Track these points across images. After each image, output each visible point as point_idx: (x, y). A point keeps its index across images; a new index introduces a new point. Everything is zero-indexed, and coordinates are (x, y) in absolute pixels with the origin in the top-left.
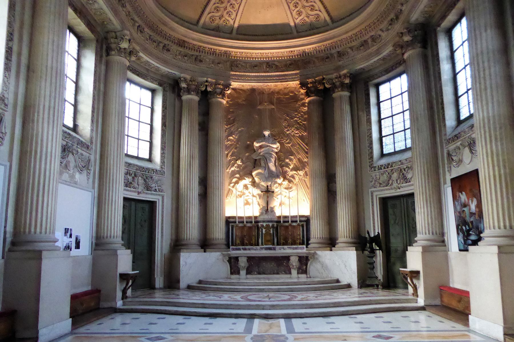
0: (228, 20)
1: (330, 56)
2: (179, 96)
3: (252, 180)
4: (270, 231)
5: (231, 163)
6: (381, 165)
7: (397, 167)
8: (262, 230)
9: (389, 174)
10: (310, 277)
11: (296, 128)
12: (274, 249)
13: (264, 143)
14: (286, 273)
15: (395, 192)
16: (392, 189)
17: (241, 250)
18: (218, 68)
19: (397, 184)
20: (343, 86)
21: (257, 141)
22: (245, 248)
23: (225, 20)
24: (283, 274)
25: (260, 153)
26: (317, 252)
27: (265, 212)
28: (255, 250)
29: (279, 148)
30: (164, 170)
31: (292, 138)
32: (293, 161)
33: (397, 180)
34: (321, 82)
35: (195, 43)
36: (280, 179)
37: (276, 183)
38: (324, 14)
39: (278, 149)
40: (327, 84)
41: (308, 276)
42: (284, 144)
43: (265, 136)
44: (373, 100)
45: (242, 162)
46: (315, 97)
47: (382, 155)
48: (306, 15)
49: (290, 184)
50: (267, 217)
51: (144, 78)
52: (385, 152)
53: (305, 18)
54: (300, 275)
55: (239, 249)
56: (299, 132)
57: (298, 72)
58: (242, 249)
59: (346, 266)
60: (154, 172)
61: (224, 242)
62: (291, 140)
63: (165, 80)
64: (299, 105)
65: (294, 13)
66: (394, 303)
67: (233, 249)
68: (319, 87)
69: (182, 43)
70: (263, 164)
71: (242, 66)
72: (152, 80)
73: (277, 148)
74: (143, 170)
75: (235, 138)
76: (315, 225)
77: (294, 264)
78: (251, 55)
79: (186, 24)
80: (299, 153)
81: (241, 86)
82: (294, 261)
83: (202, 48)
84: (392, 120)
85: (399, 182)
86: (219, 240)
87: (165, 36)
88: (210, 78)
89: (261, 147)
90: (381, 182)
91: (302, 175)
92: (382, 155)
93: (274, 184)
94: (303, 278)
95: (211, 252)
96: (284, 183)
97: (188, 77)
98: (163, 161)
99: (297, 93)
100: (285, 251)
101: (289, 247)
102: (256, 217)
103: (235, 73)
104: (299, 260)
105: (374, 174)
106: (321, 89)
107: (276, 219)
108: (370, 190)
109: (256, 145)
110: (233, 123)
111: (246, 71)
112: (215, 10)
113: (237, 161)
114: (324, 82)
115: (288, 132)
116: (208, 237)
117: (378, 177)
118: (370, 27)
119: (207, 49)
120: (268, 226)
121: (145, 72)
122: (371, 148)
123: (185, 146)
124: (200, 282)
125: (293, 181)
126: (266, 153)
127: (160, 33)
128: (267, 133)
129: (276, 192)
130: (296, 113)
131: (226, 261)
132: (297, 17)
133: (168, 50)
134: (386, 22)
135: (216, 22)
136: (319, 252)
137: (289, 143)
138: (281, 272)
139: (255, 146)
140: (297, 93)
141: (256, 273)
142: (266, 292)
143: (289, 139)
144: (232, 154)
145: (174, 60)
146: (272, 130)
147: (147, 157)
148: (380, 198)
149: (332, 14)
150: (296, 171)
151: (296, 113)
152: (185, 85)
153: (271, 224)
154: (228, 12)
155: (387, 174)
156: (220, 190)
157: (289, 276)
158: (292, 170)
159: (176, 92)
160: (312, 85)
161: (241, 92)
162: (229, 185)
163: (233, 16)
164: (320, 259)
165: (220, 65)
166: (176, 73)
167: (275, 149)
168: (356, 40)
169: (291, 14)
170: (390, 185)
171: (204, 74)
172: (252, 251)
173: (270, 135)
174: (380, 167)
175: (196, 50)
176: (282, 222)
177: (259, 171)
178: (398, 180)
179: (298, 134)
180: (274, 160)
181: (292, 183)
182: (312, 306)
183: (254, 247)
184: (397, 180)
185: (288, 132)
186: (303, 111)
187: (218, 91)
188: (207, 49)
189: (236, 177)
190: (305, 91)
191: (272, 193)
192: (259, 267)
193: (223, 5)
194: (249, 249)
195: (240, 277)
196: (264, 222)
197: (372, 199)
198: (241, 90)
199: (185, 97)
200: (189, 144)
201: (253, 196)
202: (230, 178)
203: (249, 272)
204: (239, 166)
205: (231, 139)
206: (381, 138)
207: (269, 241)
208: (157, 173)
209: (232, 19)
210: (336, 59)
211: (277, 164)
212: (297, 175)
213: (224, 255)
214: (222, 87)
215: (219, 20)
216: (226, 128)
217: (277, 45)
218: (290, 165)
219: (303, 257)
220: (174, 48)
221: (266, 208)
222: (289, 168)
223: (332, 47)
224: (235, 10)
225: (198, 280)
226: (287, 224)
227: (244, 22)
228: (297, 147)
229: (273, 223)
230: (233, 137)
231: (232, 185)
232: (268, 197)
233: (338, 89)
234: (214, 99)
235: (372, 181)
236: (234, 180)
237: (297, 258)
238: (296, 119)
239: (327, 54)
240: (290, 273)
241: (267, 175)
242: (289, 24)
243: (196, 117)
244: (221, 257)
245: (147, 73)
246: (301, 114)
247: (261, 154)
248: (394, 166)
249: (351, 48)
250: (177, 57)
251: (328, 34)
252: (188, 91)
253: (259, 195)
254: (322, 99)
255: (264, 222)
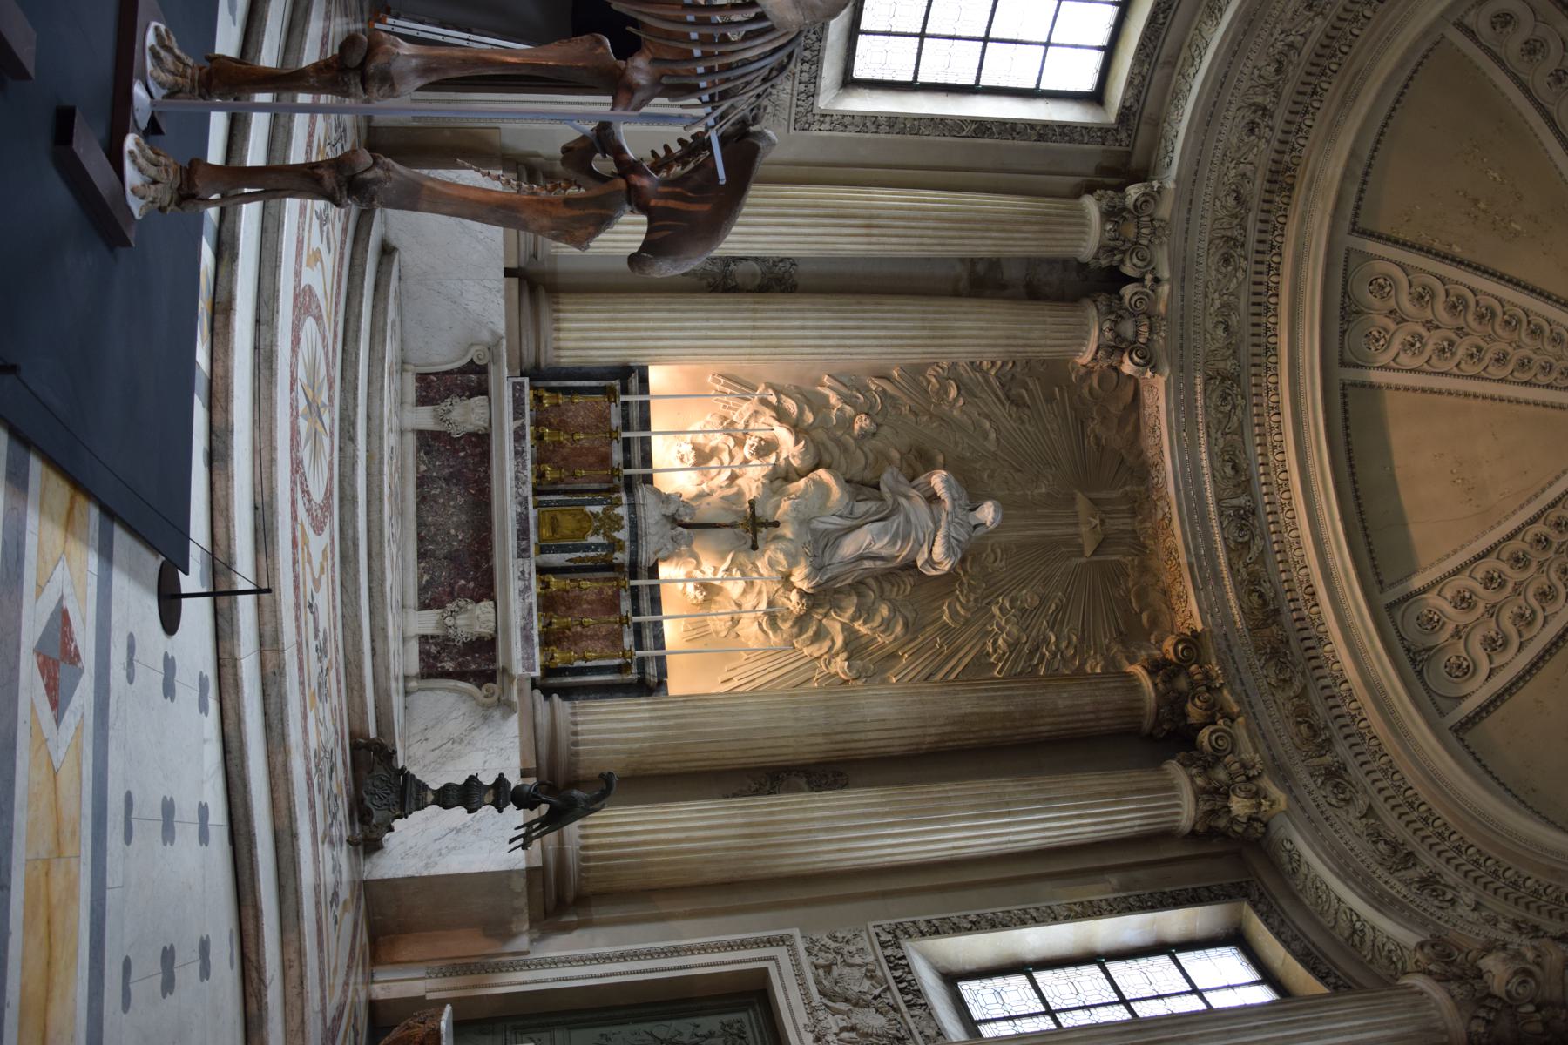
0: (1389, 343)
1: (1323, 737)
2: (1090, 189)
3: (795, 469)
4: (596, 532)
5: (855, 393)
6: (908, 965)
7: (912, 1026)
8: (600, 503)
9: (875, 998)
10: (407, 693)
11: (1019, 639)
12: (523, 553)
13: (948, 505)
14: (422, 590)
15: (801, 1026)
16: (812, 1011)
17: (515, 419)
18: (1210, 325)
19: (835, 1029)
20: (1214, 795)
21: (952, 480)
22: (524, 437)
23: (1387, 331)
24: (420, 577)
25: (908, 497)
26: (515, 717)
27: (671, 510)
28: (517, 478)
29: (933, 573)
30: (815, 126)
31: (974, 629)
32: (883, 632)
33: (853, 1029)
34: (1214, 712)
35: (1292, 230)
36: (807, 577)
37: (793, 560)
38: (1485, 688)
39: (928, 567)
40: (1213, 732)
41: (413, 684)
42: (947, 594)
43: (974, 509)
44: (1175, 922)
45: (865, 435)
46: (1153, 695)
47: (952, 979)
48: (1466, 626)
49: (789, 623)
50: (650, 521)
51: (1142, 46)
52: (966, 988)
53: (1450, 628)
54: (414, 647)
55: (518, 413)
56: (1004, 654)
57: (1239, 625)
58: (519, 423)
59: (458, 831)
60: (807, 83)
61: (549, 358)
62: (967, 622)
63: (1144, 133)
64: (1108, 649)
65: (1462, 581)
66: (283, 961)
67: (518, 389)
68: (1195, 705)
69: (1282, 180)
70: (862, 508)
71: (1228, 416)
72: (1138, 82)
73: (930, 561)
74: (814, 37)
75: (953, 404)
76: (653, 329)
77: (461, 621)
78: (1274, 448)
79: (1355, 190)
80: (916, 654)
81: (1151, 422)
82: (474, 619)
83: (1276, 259)
84: (1106, 1001)
85: (845, 1035)
86: (555, 335)
87: (1301, 109)
88: (1171, 290)
89: (932, 499)
90: (835, 971)
91: (833, 670)
92: (952, 979)
93: (787, 554)
94: (406, 660)
95: (507, 299)
96: (794, 596)
97: (1165, 210)
98: (847, 120)
99: (1153, 641)
100: (517, 592)
101: (530, 609)
102: (648, 479)
103: (1199, 389)
104: (480, 639)
105: (868, 945)
106: (1185, 716)
107: (645, 558)
108: (796, 932)
109: (938, 480)
110: (1008, 398)
111: (1213, 431)
112: (1420, 289)
113: (867, 414)
114: (1221, 722)
115: (995, 610)
116: (564, 299)
117: (857, 959)
118: (1475, 862)
119: (1274, 279)
120: (616, 523)
121: (1167, 50)
122: (975, 927)
123: (912, 201)
124: (387, 251)
125: (804, 637)
126: (908, 520)
127: (1294, 128)
128: (988, 513)
129: (754, 564)
130: (1074, 638)
131: (472, 354)
132: (1448, 593)
133: (1252, 128)
134: (1519, 912)
135: (1376, 302)
136: (512, 726)
137: (954, 614)
138: (426, 570)
139: (931, 475)
140: (1153, 641)
141: (423, 468)
142: (341, 449)
143: (969, 615)
144: (892, 397)
145: (1219, 153)
146: (999, 551)
147: (861, 71)
148: (765, 971)
149: (1490, 723)
150: (846, 644)
151: (1074, 638)
152: (1135, 197)
153: (623, 535)
154: (1421, 338)
155: (876, 992)
156: (749, 333)
157: (412, 598)
158: (846, 628)
159: (1099, 179)
160: (1197, 677)
161: (1129, 429)
162: (769, 386)
163: (1405, 360)
164: (485, 730)
165: (1220, 332)
166: (1170, 178)
167: (926, 556)
168: (1408, 823)
169: (1456, 572)
170: (830, 1004)
171: (1182, 278)
172: (513, 463)
173: (980, 532)
174: (903, 962)
175: (1263, 236)
176: (633, 583)
177: (836, 491)
178: (853, 1035)
179: (995, 651)
180: (884, 552)
181: (795, 630)
182: (271, 681)
183: (529, 474)
184: (853, 1029)
185: (995, 610)
186: (1085, 663)
187: (1127, 328)
188: (1274, 279)
189: (801, 412)
190: (1171, 656)
191: (749, 543)
192: (447, 480)
193: (1443, 315)
194: (518, 454)
195: (408, 407)
196: (632, 507)
197: (757, 943)
198: (1137, 428)
199: (1091, 206)
200: (919, 214)
201: (733, 478)
202: (796, 387)
203: (427, 441)
204: (847, 423)
205: (947, 393)
206: (1023, 967)
207: (555, 526)
208: (803, 96)
209: (1398, 360)
210: (1316, 761)
211: (868, 564)
212: (830, 649)
213: (493, 348)
214: (1142, 340)
215: (1386, 312)
216: (987, 372)
217: (1328, 533)
218: (865, 623)
219: (493, 660)
220: (1262, 152)
221: (687, 520)
222: (853, 619)
223: (1360, 739)
224: (1434, 361)
225: (394, 243)
226: (626, 605)
227: (1394, 405)
228: (941, 646)
229: (627, 544)
230: (956, 400)
231: (773, 399)
232: (732, 526)
233: (1200, 775)
234: (1094, 312)
235: (834, 938)
236: (790, 405)
237: (484, 629)
238: (1053, 639)
239: (1326, 727)
240: (424, 606)
241: (822, 526)
242: (1415, 572)
243: (1023, 245)
244: (486, 336)
245: (1161, 60)
246: (1074, 656)
247: (903, 500)
248: (916, 1012)
249: (1370, 812)
250: (1233, 165)
251: (1408, 712)
252: (1112, 214)
253: (740, 494)
254: (1147, 724)
255: (632, 507)
